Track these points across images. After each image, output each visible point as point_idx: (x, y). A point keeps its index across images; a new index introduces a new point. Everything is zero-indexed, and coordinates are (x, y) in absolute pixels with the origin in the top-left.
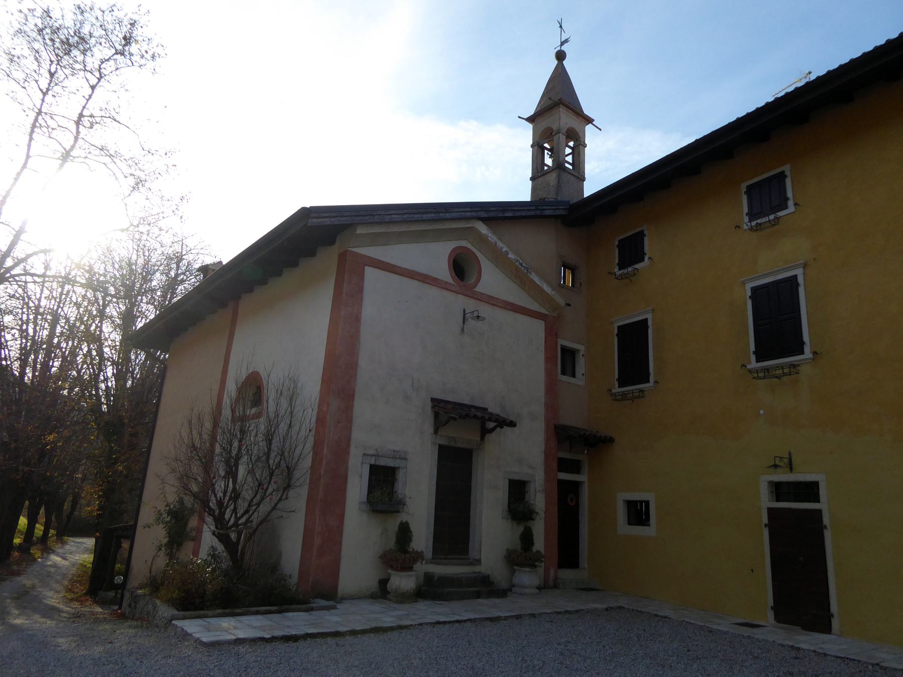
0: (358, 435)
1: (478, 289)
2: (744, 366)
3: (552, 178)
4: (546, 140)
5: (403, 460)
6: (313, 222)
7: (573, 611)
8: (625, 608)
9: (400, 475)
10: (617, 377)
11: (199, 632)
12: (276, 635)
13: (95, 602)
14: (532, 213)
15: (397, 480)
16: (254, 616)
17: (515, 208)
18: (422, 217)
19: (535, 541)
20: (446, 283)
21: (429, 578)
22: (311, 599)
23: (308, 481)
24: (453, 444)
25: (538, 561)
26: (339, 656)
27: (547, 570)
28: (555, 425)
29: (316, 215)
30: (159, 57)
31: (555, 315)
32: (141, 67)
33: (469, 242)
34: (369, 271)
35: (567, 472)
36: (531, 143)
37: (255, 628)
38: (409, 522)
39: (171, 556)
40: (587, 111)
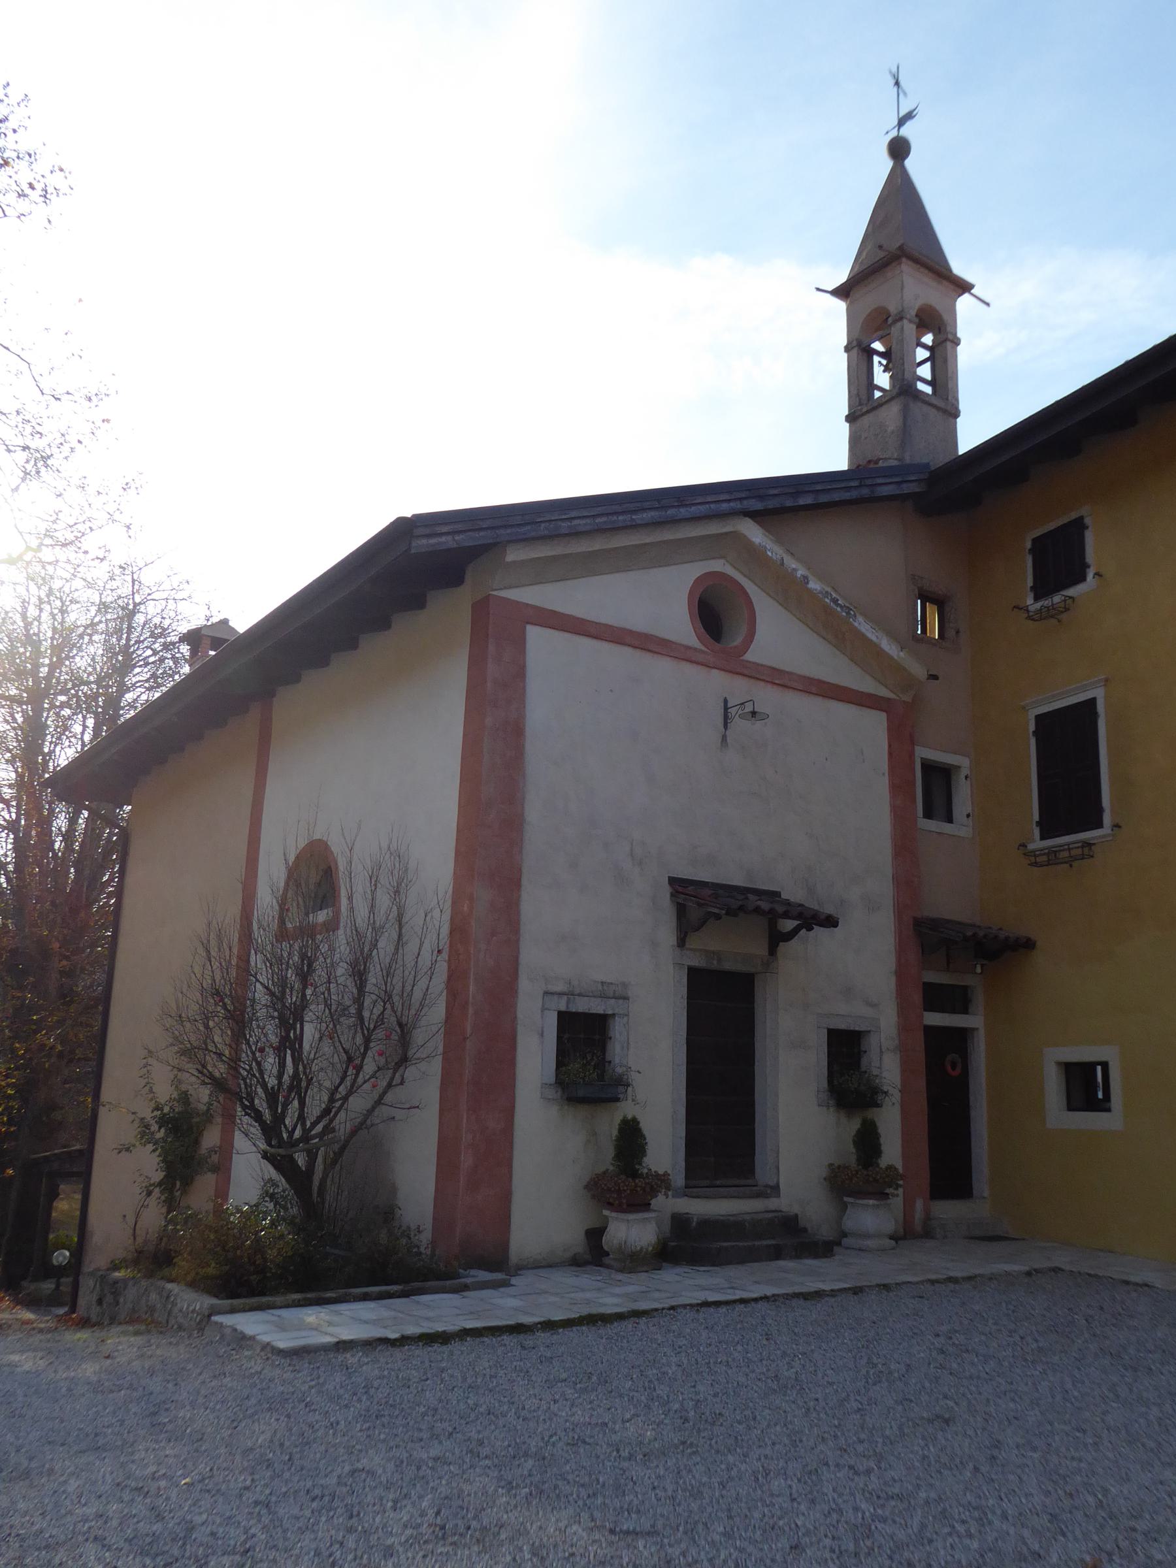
0: (532, 955)
1: (749, 656)
2: (1024, 846)
3: (891, 416)
4: (875, 335)
5: (621, 1001)
6: (421, 544)
7: (963, 1278)
8: (1063, 1270)
9: (617, 1030)
10: (1036, 817)
11: (266, 1333)
12: (409, 1333)
13: (18, 1302)
14: (854, 494)
15: (610, 1038)
16: (361, 1303)
17: (819, 487)
18: (633, 520)
19: (883, 1148)
20: (688, 648)
21: (680, 1223)
22: (461, 1271)
23: (441, 1049)
24: (715, 965)
25: (890, 1187)
26: (529, 1365)
27: (908, 1204)
28: (915, 918)
29: (427, 531)
30: (58, 196)
31: (907, 698)
32: (22, 217)
33: (727, 561)
34: (534, 634)
35: (943, 1011)
36: (845, 343)
37: (366, 1322)
38: (639, 1118)
39: (171, 1204)
40: (959, 267)
